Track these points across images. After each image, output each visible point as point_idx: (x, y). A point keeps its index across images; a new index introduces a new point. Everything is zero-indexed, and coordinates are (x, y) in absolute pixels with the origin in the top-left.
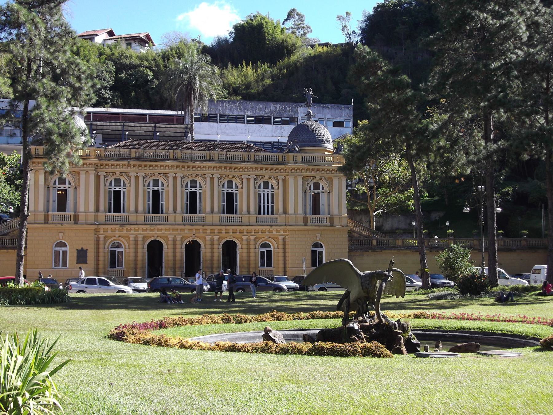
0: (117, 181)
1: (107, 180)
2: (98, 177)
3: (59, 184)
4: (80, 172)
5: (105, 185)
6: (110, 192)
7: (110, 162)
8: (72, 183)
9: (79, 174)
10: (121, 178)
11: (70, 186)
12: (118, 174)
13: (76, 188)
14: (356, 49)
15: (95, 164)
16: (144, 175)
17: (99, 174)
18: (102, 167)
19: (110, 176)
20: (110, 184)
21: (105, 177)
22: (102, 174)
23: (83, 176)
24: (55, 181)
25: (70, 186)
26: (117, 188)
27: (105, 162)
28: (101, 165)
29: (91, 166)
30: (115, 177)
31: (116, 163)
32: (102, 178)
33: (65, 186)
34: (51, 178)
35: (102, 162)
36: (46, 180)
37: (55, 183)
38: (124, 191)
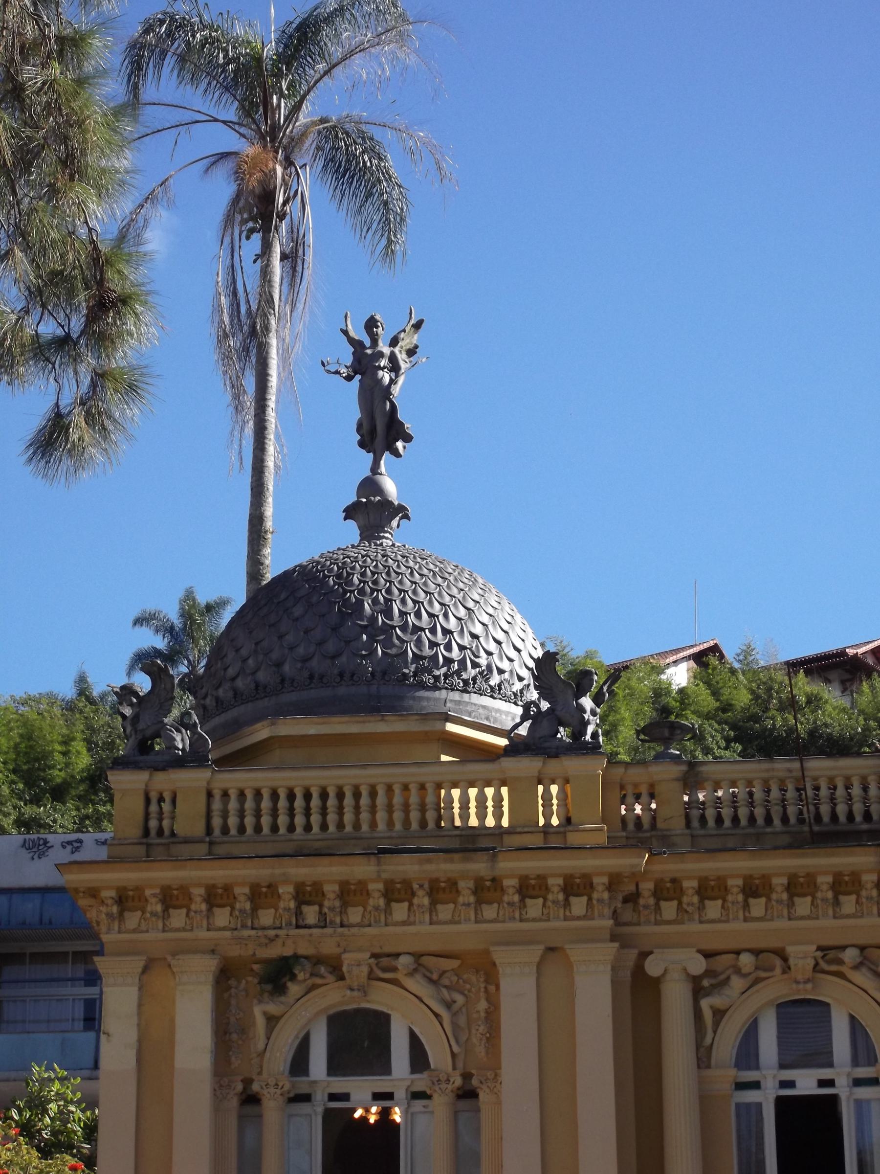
0: (803, 1023)
1: (719, 1014)
2: (640, 994)
3: (335, 1067)
4: (500, 955)
5: (703, 1057)
6: (749, 1115)
7: (737, 866)
8: (438, 1055)
9: (489, 973)
10: (830, 991)
11: (421, 1082)
12: (802, 956)
13: (467, 1094)
14: (91, 304)
15: (614, 881)
16: (698, 965)
17: (653, 967)
18: (669, 909)
19: (737, 983)
20: (747, 1054)
21: (698, 991)
22: (675, 965)
23: (517, 991)
24: (751, 1035)
25: (421, 1082)
26: (806, 1083)
27: (692, 868)
28: (660, 894)
29: (578, 905)
30: (776, 989)
31: (779, 865)
32: (676, 999)
33: (826, 1073)
34: (272, 1021)
35: (668, 867)
36: (227, 1033)
37: (300, 1063)
38: (859, 1104)
